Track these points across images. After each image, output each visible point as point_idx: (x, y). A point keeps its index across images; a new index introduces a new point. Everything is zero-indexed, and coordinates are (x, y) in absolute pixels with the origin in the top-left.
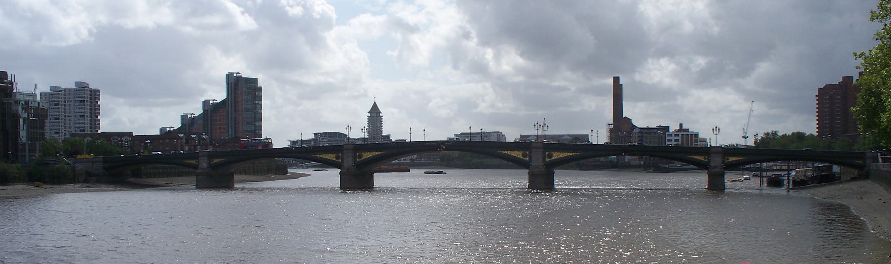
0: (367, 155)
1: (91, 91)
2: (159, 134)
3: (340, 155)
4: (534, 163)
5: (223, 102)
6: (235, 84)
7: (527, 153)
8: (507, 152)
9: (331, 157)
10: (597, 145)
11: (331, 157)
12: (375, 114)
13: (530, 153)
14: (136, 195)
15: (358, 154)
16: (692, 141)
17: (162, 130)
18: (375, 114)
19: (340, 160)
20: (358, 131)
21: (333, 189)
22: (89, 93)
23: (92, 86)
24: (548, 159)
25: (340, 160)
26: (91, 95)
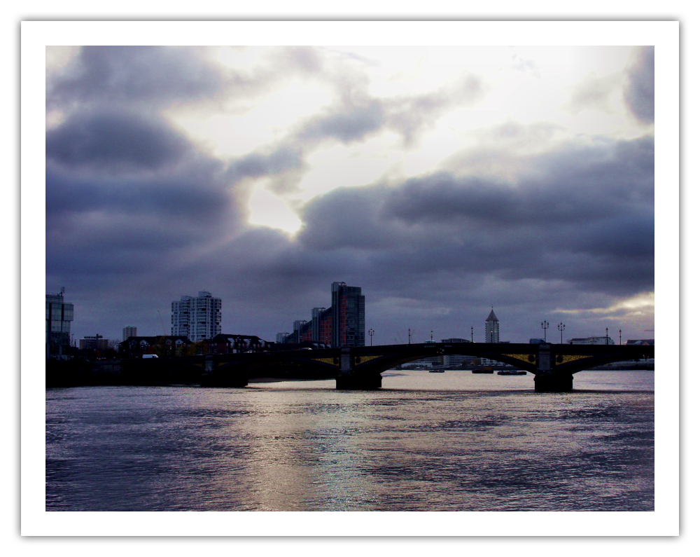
0: (567, 359)
1: (212, 300)
2: (484, 341)
3: (534, 356)
4: (541, 368)
5: (330, 309)
6: (339, 293)
7: (534, 356)
8: (511, 356)
9: (524, 358)
10: (409, 345)
11: (524, 358)
12: (492, 319)
13: (537, 356)
14: (107, 390)
15: (557, 356)
16: (131, 332)
17: (531, 340)
18: (492, 319)
19: (534, 363)
20: (480, 338)
21: (333, 390)
22: (210, 301)
23: (215, 296)
24: (557, 363)
25: (534, 363)
26: (212, 304)
